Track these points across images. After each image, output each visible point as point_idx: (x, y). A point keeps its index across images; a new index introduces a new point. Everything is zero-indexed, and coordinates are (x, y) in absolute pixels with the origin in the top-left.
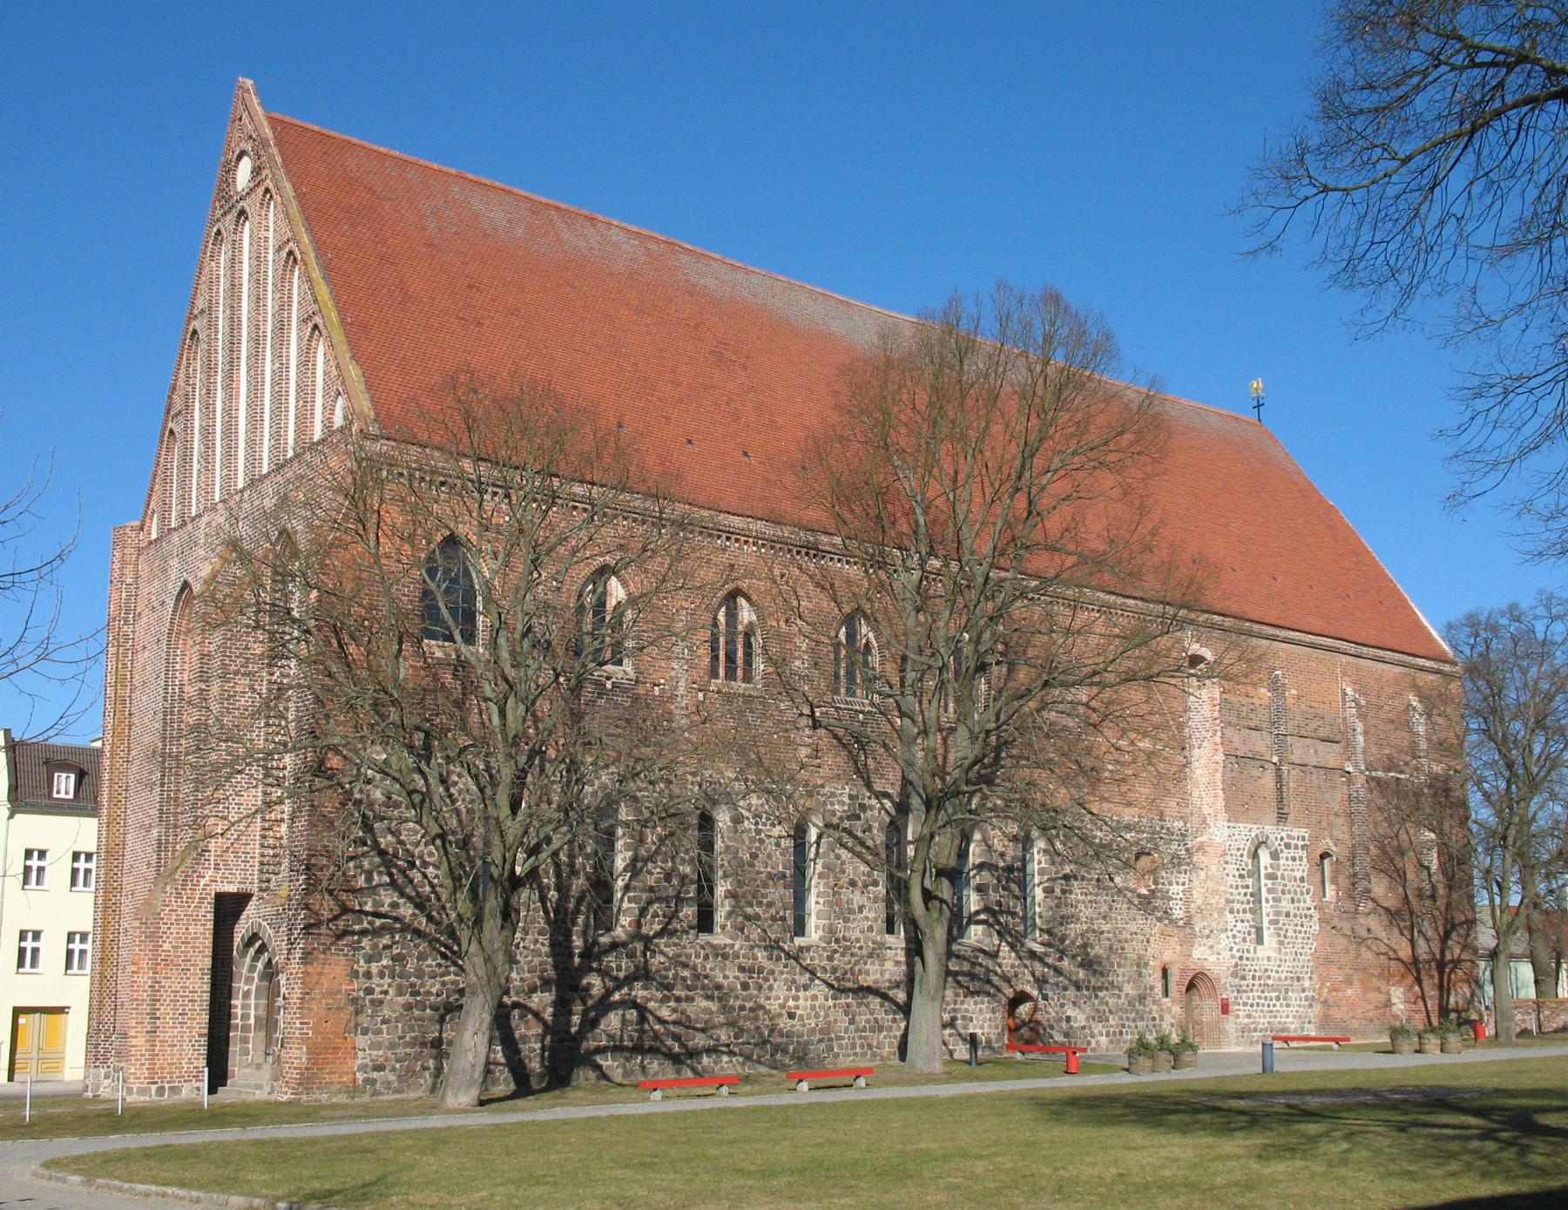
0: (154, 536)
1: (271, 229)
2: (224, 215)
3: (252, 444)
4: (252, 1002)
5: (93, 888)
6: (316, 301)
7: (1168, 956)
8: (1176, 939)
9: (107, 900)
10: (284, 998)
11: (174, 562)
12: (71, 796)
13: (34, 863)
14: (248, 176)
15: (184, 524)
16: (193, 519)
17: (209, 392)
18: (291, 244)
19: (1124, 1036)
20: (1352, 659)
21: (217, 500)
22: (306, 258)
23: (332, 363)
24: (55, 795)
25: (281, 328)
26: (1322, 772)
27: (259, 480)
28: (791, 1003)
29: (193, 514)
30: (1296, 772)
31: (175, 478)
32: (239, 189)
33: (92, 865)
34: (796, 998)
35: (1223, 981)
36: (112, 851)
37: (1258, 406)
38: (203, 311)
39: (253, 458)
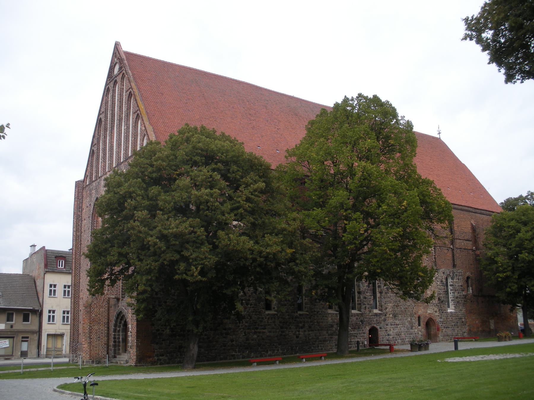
0: (88, 183)
1: (125, 86)
2: (110, 82)
3: (118, 153)
4: (121, 334)
5: (70, 297)
6: (138, 106)
7: (420, 313)
8: (422, 307)
9: (74, 300)
10: (131, 333)
11: (94, 191)
12: (63, 267)
13: (53, 288)
14: (118, 70)
15: (96, 180)
16: (99, 178)
17: (105, 137)
18: (131, 89)
19: (406, 340)
20: (473, 214)
21: (107, 171)
22: (135, 93)
23: (143, 125)
24: (58, 267)
25: (128, 115)
26: (466, 250)
27: (120, 164)
28: (297, 333)
29: (100, 176)
30: (458, 251)
31: (94, 165)
32: (115, 74)
33: (70, 289)
34: (299, 331)
35: (437, 320)
36: (76, 285)
37: (439, 133)
38: (103, 112)
39: (119, 157)
